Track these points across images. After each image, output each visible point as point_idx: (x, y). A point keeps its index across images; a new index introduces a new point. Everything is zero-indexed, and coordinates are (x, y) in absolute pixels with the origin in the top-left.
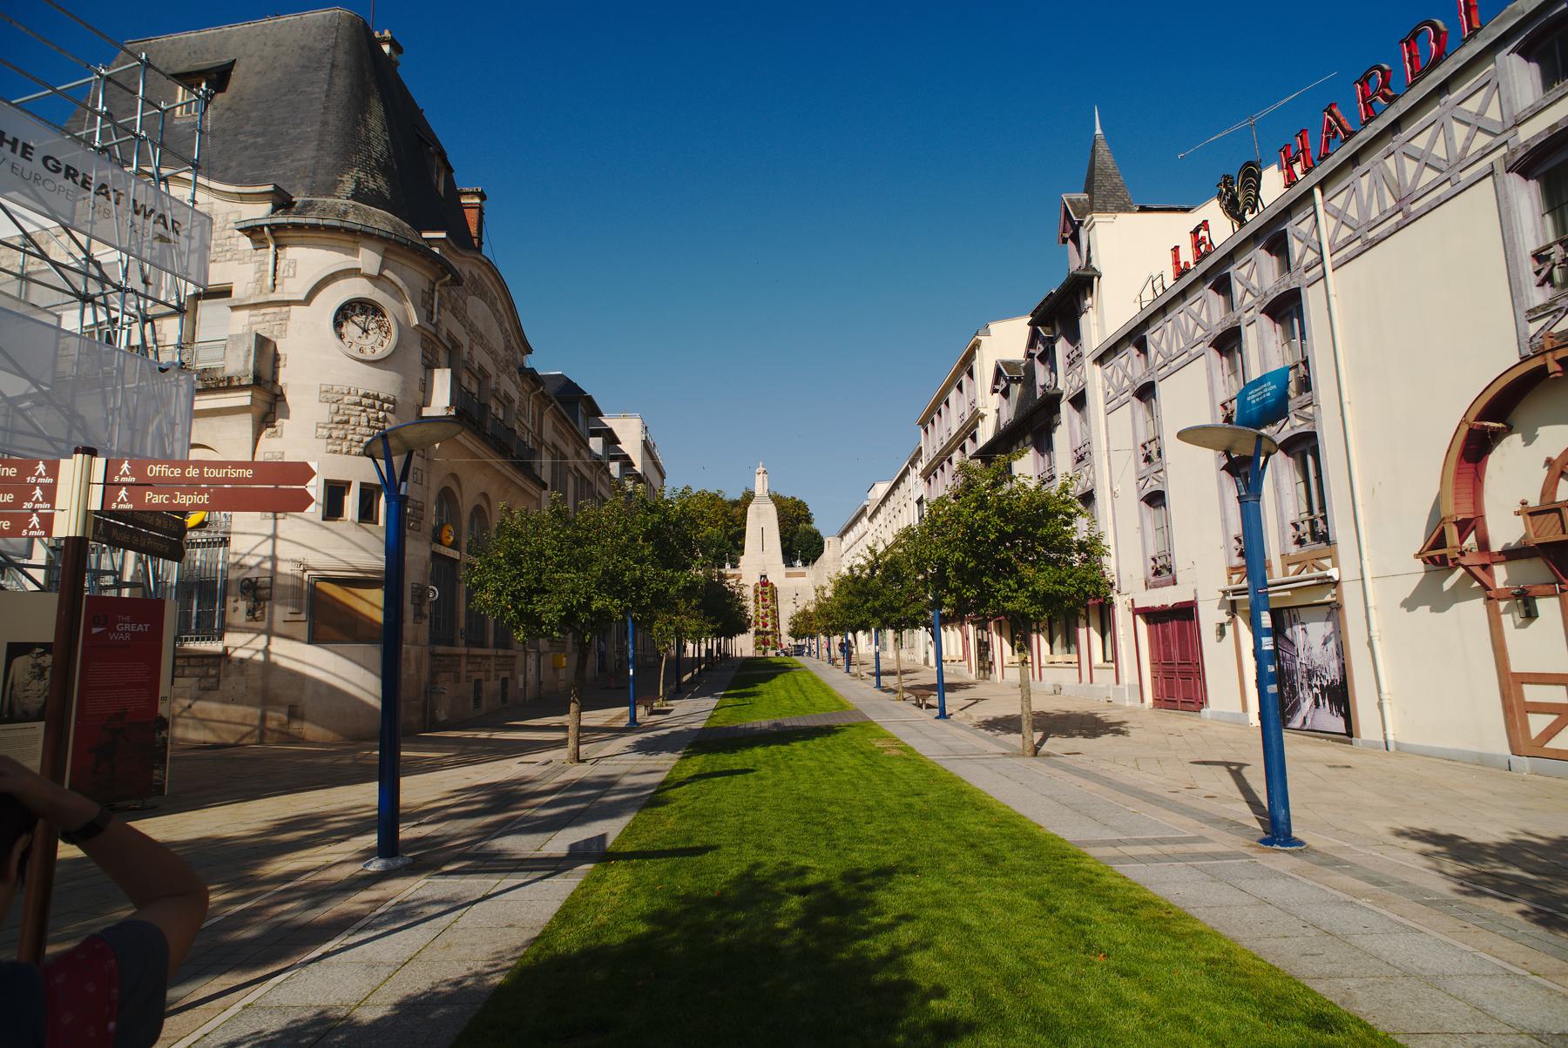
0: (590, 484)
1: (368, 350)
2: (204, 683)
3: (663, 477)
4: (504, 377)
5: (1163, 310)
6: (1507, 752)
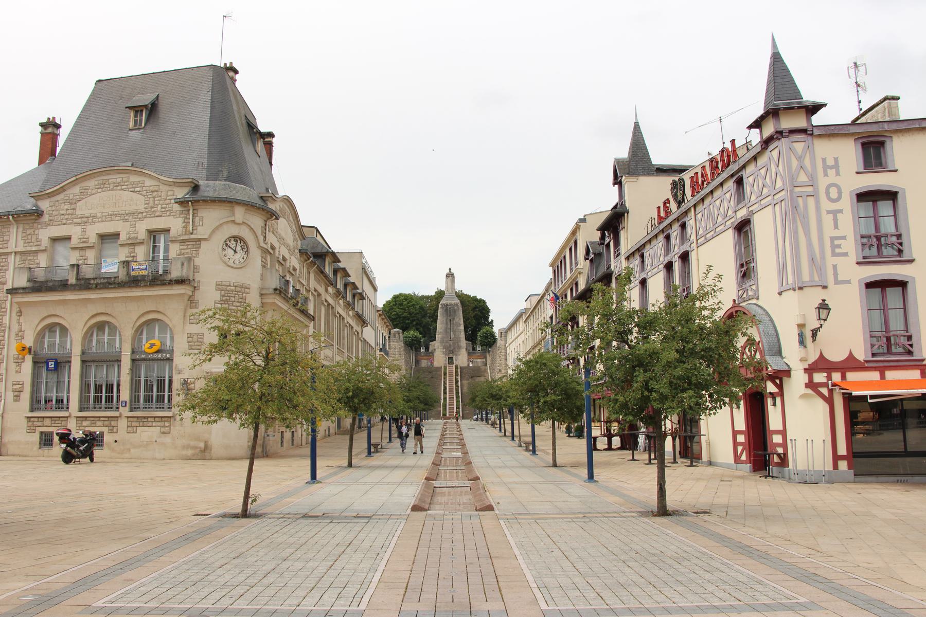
0: (333, 308)
1: (237, 262)
2: (163, 430)
3: (375, 290)
4: (293, 257)
5: (650, 241)
6: (733, 462)
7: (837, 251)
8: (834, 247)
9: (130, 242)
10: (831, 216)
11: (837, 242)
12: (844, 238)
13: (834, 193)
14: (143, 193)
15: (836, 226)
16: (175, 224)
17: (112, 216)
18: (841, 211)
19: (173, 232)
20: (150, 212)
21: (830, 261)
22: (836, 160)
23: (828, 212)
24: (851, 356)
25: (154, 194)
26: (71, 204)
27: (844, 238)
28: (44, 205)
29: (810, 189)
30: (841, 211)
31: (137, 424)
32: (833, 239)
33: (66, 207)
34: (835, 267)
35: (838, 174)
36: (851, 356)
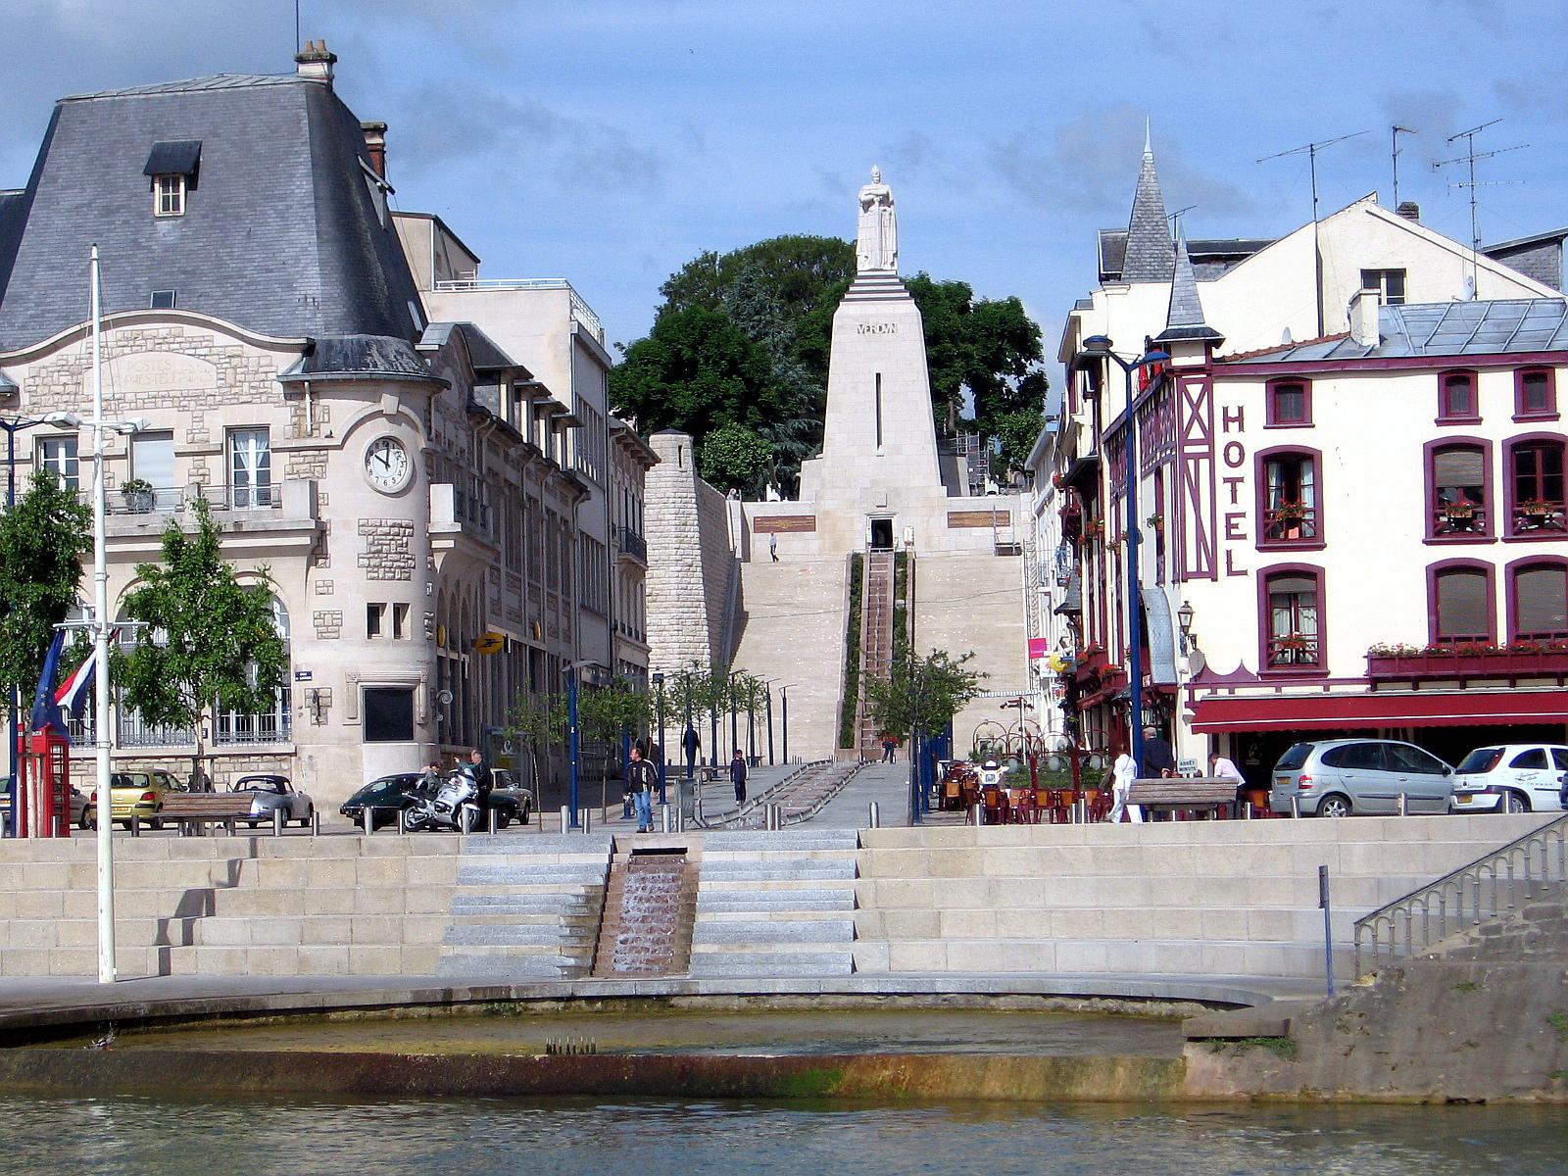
7: (1234, 532)
8: (1229, 526)
9: (195, 448)
10: (1228, 486)
11: (1234, 521)
12: (1243, 515)
13: (1234, 453)
14: (215, 359)
15: (1234, 500)
16: (279, 417)
17: (156, 400)
18: (1241, 480)
19: (277, 439)
20: (230, 396)
21: (1223, 544)
22: (1241, 410)
23: (1226, 480)
24: (1242, 670)
25: (235, 361)
26: (72, 375)
27: (1243, 515)
28: (121, 444)
29: (1205, 449)
30: (1241, 480)
31: (229, 767)
32: (1229, 516)
33: (63, 379)
34: (1229, 553)
35: (1241, 428)
36: (1242, 670)
